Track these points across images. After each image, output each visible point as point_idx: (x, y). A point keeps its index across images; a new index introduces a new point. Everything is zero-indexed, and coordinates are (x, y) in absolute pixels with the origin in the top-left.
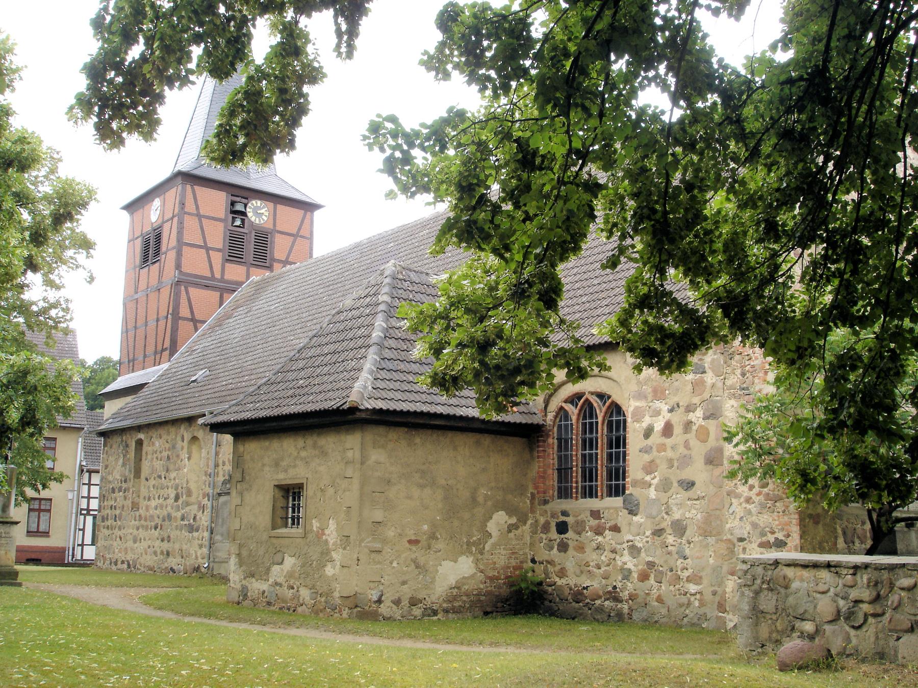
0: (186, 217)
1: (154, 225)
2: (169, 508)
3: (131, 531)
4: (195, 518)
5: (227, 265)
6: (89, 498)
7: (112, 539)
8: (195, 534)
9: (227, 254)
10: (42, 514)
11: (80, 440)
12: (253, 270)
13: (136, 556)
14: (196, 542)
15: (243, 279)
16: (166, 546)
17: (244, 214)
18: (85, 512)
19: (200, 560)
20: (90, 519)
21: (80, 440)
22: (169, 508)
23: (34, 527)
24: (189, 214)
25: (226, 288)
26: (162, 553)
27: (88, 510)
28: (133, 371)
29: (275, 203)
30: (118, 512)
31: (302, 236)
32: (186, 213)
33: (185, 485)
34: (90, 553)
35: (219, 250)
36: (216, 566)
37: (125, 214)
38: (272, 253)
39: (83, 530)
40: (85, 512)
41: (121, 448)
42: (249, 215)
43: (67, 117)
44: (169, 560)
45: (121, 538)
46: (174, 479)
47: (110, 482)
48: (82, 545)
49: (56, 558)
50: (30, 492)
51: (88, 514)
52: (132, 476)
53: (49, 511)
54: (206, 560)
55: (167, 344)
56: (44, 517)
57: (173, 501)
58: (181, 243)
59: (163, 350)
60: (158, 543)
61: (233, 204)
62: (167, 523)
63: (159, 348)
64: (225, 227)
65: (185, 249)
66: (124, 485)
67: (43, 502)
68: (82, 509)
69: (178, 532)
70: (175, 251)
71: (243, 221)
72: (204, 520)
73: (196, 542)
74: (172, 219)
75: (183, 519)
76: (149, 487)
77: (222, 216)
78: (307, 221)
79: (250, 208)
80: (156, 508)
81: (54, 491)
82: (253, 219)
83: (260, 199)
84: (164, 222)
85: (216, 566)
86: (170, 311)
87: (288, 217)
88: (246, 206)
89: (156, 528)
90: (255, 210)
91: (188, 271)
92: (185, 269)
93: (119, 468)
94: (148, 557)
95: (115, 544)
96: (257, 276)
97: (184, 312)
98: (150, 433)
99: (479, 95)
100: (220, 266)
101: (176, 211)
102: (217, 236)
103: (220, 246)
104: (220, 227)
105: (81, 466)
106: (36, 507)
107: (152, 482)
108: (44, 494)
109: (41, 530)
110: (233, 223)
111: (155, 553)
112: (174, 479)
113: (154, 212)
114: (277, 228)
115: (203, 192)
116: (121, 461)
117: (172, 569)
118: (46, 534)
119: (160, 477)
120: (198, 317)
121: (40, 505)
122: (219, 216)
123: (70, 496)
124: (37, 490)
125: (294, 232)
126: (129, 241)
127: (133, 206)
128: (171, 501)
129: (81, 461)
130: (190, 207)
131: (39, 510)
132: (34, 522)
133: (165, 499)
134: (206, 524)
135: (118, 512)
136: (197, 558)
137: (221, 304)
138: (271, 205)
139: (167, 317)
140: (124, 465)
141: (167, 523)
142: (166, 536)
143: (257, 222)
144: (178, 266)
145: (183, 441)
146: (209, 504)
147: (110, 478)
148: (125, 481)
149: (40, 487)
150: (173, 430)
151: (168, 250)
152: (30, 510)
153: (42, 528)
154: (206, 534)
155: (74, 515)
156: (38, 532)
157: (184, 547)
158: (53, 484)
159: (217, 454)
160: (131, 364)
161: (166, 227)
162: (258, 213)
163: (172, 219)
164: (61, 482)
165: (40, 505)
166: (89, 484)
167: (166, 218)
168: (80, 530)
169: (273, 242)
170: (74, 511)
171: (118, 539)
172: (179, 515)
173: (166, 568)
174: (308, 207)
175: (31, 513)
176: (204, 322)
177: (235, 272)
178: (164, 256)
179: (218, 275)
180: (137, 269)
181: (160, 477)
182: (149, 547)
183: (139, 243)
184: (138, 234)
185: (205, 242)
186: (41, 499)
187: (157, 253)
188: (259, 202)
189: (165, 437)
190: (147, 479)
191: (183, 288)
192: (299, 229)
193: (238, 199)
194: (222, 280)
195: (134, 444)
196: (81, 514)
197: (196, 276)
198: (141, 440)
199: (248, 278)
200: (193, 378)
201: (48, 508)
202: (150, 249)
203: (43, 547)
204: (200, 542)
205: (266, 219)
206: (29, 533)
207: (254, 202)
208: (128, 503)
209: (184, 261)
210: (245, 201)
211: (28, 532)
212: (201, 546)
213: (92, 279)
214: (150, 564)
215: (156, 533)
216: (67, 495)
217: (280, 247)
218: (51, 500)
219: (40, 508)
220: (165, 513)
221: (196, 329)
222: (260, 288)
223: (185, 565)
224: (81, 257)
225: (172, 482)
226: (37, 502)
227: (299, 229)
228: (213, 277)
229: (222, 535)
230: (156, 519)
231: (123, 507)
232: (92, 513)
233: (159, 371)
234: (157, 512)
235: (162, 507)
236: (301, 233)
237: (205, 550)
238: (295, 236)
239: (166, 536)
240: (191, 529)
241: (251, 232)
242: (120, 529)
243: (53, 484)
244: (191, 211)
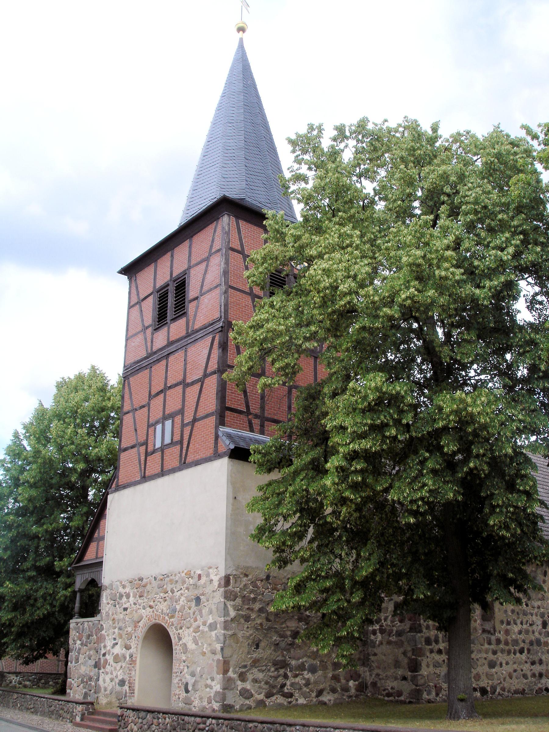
2: (536, 634)
3: (485, 655)
16: (537, 668)
22: (536, 634)
26: (534, 675)
43: (294, 137)
57: (540, 627)
60: (526, 668)
80: (520, 632)
84: (190, 268)
99: (350, 120)
111: (525, 676)
133: (531, 625)
180: (149, 331)
182: (515, 671)
214: (520, 687)
225: (536, 610)
234: (522, 636)
235: (527, 632)
239: (537, 659)
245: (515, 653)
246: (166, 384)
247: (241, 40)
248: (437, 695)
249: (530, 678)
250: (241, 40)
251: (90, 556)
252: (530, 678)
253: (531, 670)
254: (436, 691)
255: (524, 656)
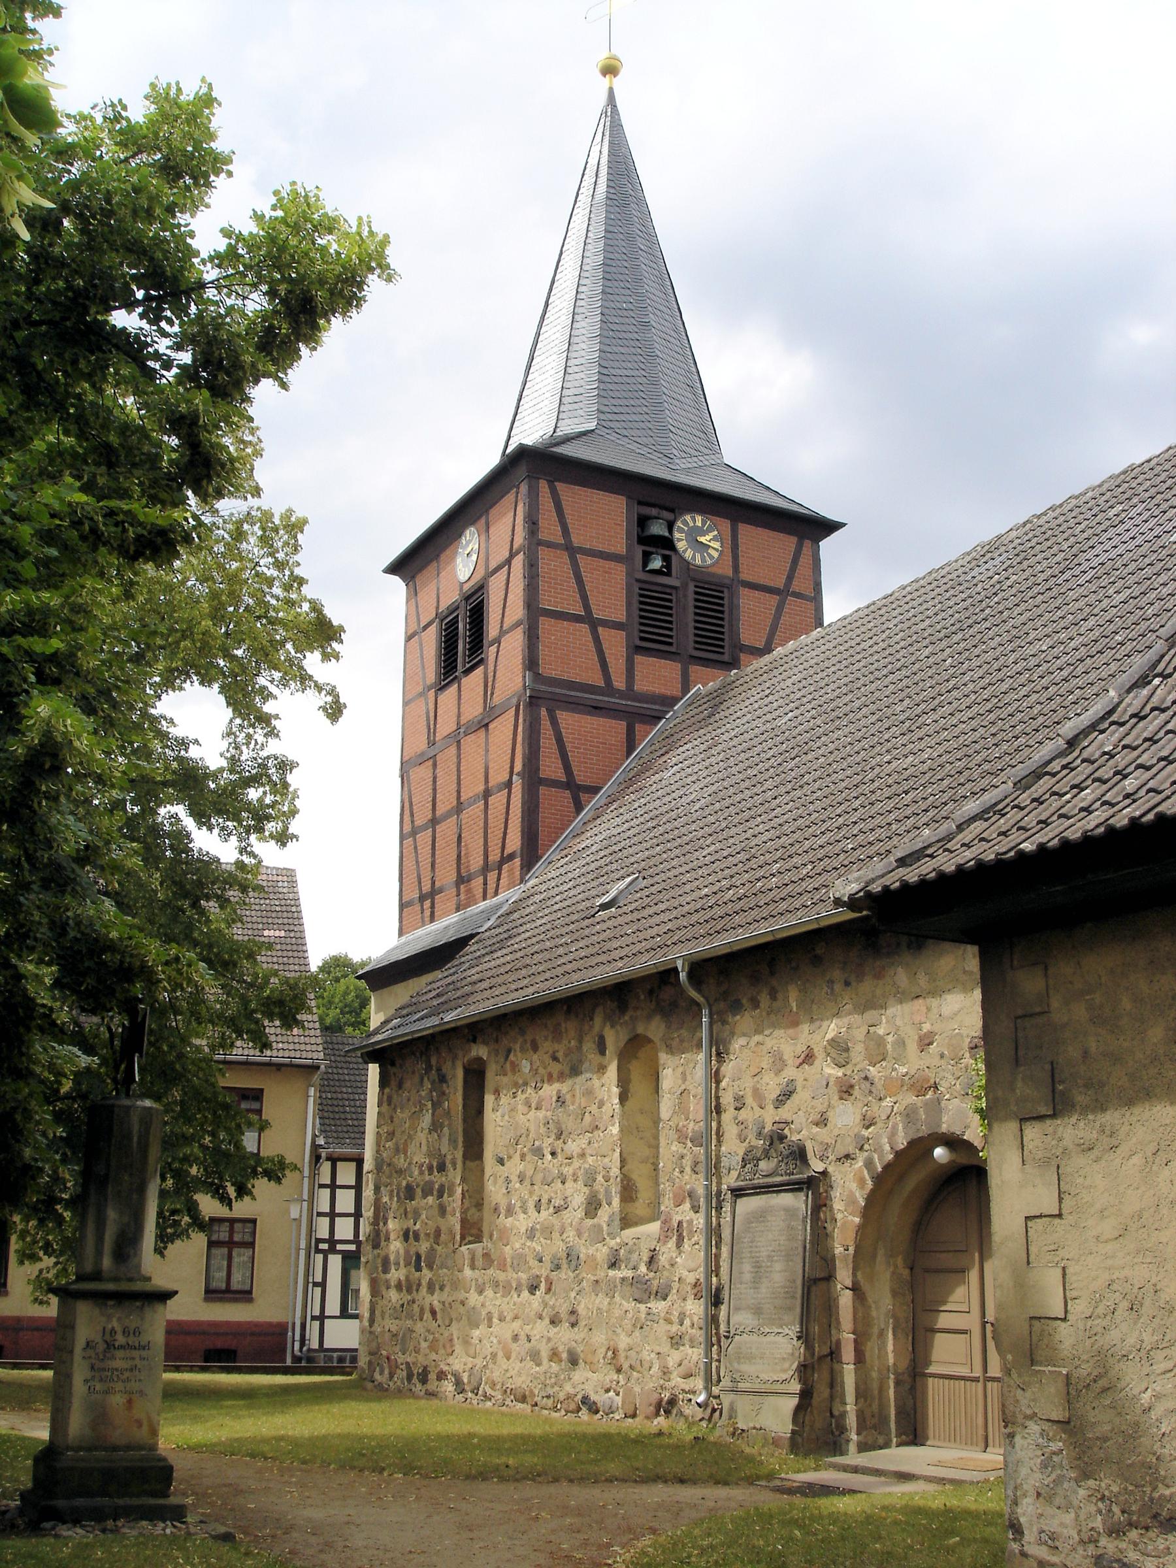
0: (543, 552)
1: (466, 587)
2: (571, 1234)
4: (652, 1261)
5: (638, 658)
6: (332, 1215)
7: (410, 1316)
8: (658, 1306)
9: (636, 634)
10: (235, 1252)
11: (312, 1091)
12: (696, 670)
13: (479, 1362)
14: (662, 1329)
15: (674, 689)
16: (564, 1336)
17: (667, 544)
18: (324, 1246)
19: (676, 1381)
20: (335, 1262)
21: (312, 1091)
23: (219, 1282)
24: (549, 545)
25: (640, 713)
26: (554, 1355)
27: (332, 1242)
28: (432, 919)
29: (735, 521)
30: (424, 1247)
31: (800, 595)
32: (540, 543)
33: (615, 1171)
34: (343, 1335)
35: (618, 626)
36: (744, 1405)
37: (397, 583)
38: (735, 633)
39: (323, 1285)
40: (324, 1246)
41: (428, 1085)
42: (681, 545)
44: (579, 1375)
45: (433, 1313)
46: (583, 1155)
47: (400, 1172)
48: (322, 1318)
49: (265, 1348)
50: (208, 1206)
51: (332, 1250)
52: (459, 1154)
53: (251, 1245)
54: (698, 1383)
55: (514, 842)
56: (240, 1256)
57: (580, 1214)
58: (534, 610)
59: (506, 859)
60: (541, 1328)
61: (643, 521)
62: (566, 1274)
63: (495, 856)
64: (629, 574)
65: (544, 623)
66: (438, 1179)
67: (238, 1226)
68: (319, 1241)
69: (602, 1301)
70: (520, 630)
71: (666, 559)
72: (687, 1263)
73: (662, 1329)
74: (508, 562)
75: (613, 1265)
76: (508, 1180)
77: (621, 547)
78: (805, 560)
79: (681, 531)
80: (531, 1234)
81: (264, 1202)
82: (688, 555)
83: (701, 511)
85: (744, 1405)
86: (518, 767)
87: (766, 553)
88: (670, 526)
89: (533, 1289)
90: (693, 536)
91: (553, 674)
92: (546, 669)
93: (422, 1136)
94: (515, 1366)
95: (419, 1327)
96: (706, 682)
97: (551, 767)
98: (505, 1041)
100: (622, 662)
101: (519, 540)
102: (611, 593)
103: (621, 616)
104: (619, 573)
105: (315, 1147)
106: (224, 1236)
107: (515, 1167)
108: (242, 1208)
109: (235, 1286)
110: (645, 564)
111: (535, 1356)
112: (583, 1155)
113: (464, 563)
114: (744, 576)
115: (576, 497)
116: (427, 1119)
117: (585, 1400)
118: (245, 1295)
119: (538, 1152)
120: (581, 778)
121: (232, 1231)
122: (612, 550)
123: (294, 1212)
124: (225, 1200)
125: (780, 583)
126: (409, 638)
127: (410, 564)
128: (575, 1214)
129: (314, 1136)
130: (550, 529)
131: (231, 1244)
132: (219, 1269)
133: (557, 1210)
134: (691, 1278)
135: (424, 1247)
136: (666, 1372)
137: (630, 749)
138: (726, 525)
139: (509, 784)
140: (435, 1127)
141: (566, 1274)
142: (564, 1310)
143: (698, 561)
144: (531, 663)
145: (602, 1052)
146: (700, 1221)
147: (401, 1162)
148: (442, 1168)
149: (231, 1191)
150: (570, 1027)
151: (502, 633)
152: (211, 1244)
153: (238, 1280)
154: (696, 1308)
155: (302, 1253)
156: (228, 1290)
157: (623, 1342)
158: (261, 1186)
159: (717, 1077)
160: (427, 904)
161: (496, 585)
162: (701, 543)
163: (508, 562)
164: (279, 1180)
165: (232, 1231)
166: (333, 1186)
167: (493, 565)
168: (315, 1284)
169: (734, 608)
170: (303, 1245)
171: (427, 1315)
172: (601, 1252)
173: (569, 1397)
174: (813, 528)
175: (214, 1251)
176: (595, 790)
177: (656, 675)
178: (493, 649)
179: (619, 683)
181: (538, 1152)
182: (516, 1338)
183: (431, 639)
184: (428, 614)
185: (587, 606)
186: (232, 1221)
187: (477, 642)
188: (699, 519)
189: (547, 1046)
190: (501, 1162)
191: (543, 712)
192: (790, 578)
193: (654, 512)
194: (629, 692)
195: (460, 1073)
196: (318, 1251)
197: (571, 685)
198: (479, 1059)
199: (686, 689)
200: (605, 899)
201: (248, 1238)
202: (459, 641)
203: (239, 1324)
204: (675, 1328)
205: (716, 555)
206: (212, 1294)
207: (688, 518)
208: (455, 1222)
209: (543, 651)
210: (670, 516)
211: (208, 1291)
212: (676, 1341)
213: (335, 711)
214: (520, 1382)
215: (535, 1301)
216: (288, 1211)
217: (751, 614)
218: (254, 1221)
219: (234, 1239)
220: (559, 1247)
221: (579, 808)
222: (716, 701)
223: (629, 1392)
224: (312, 662)
225: (576, 1163)
226: (225, 1227)
227: (790, 578)
228: (609, 689)
229: (758, 1311)
230: (533, 1263)
231: (438, 1232)
232: (339, 1247)
233: (499, 906)
235: (548, 1231)
236: (796, 586)
237: (695, 1354)
238: (782, 593)
240: (645, 1291)
241: (685, 586)
242: (431, 1288)
243: (261, 1186)
244: (552, 539)
245: (518, 1289)
246: (577, 619)
247: (611, 92)
248: (391, 1376)
249: (545, 1361)
250: (611, 92)
251: (363, 1016)
252: (545, 1361)
253: (549, 1339)
254: (390, 1367)
255: (536, 1301)
